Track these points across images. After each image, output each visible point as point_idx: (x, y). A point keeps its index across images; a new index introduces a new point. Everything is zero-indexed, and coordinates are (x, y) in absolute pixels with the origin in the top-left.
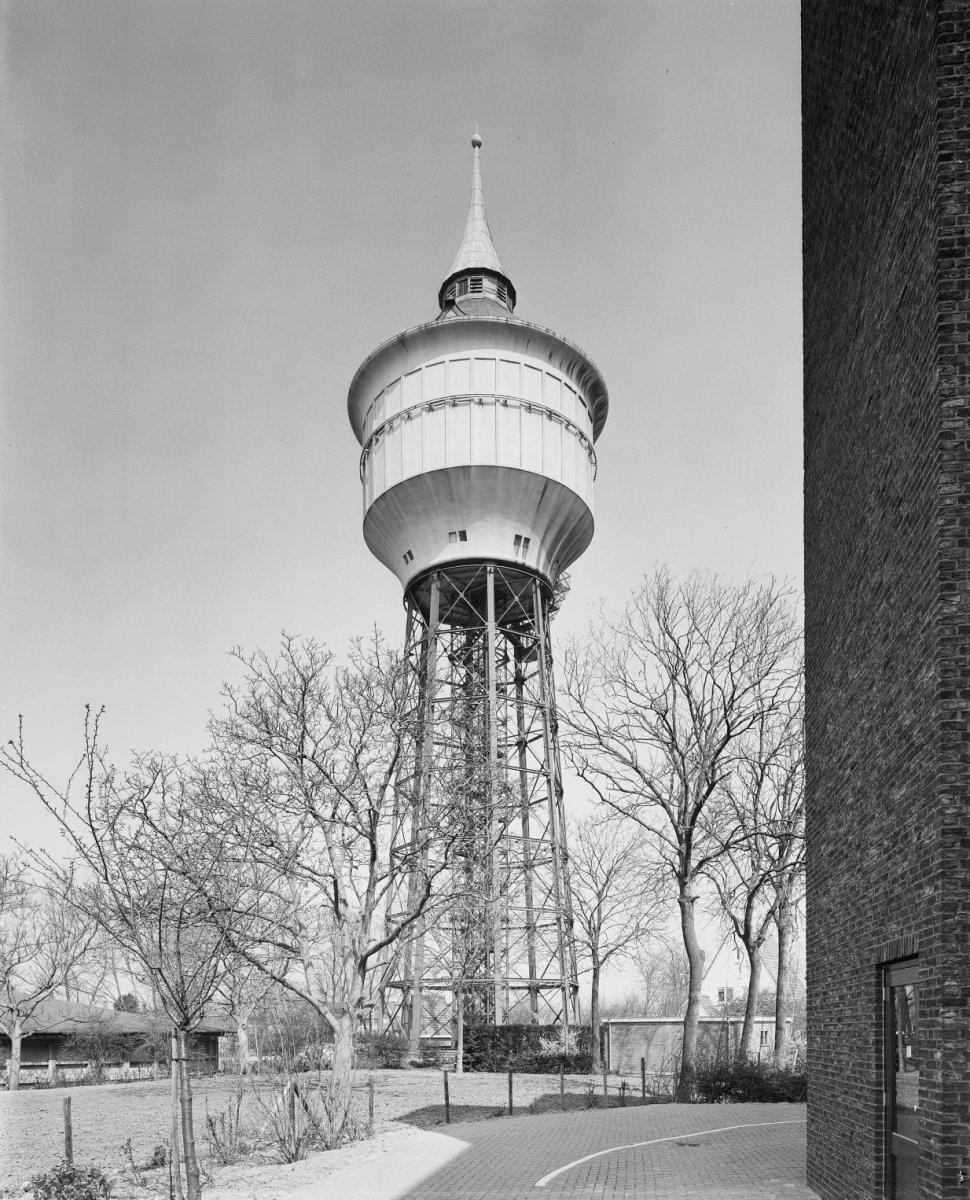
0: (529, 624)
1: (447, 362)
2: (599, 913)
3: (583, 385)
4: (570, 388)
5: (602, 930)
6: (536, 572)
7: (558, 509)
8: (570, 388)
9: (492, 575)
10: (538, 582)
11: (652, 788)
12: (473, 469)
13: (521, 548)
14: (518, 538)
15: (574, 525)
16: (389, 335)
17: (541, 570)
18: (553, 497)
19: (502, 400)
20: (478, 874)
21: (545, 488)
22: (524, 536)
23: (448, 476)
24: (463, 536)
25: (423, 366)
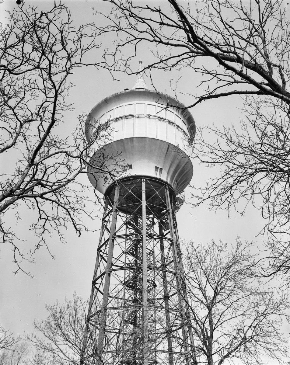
0: (165, 213)
1: (124, 106)
2: (211, 322)
3: (184, 117)
4: (178, 116)
5: (214, 339)
6: (166, 183)
7: (175, 158)
8: (178, 116)
9: (145, 183)
10: (167, 187)
11: (236, 165)
12: (134, 139)
13: (158, 172)
14: (157, 168)
15: (183, 165)
16: (101, 99)
17: (169, 182)
18: (172, 153)
19: (148, 116)
20: (138, 296)
21: (168, 148)
22: (160, 167)
23: (123, 142)
24: (131, 167)
25: (114, 108)
